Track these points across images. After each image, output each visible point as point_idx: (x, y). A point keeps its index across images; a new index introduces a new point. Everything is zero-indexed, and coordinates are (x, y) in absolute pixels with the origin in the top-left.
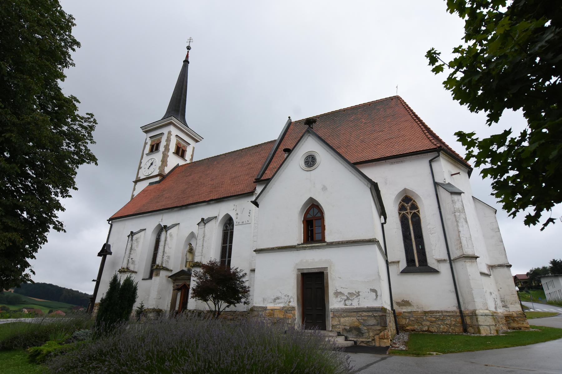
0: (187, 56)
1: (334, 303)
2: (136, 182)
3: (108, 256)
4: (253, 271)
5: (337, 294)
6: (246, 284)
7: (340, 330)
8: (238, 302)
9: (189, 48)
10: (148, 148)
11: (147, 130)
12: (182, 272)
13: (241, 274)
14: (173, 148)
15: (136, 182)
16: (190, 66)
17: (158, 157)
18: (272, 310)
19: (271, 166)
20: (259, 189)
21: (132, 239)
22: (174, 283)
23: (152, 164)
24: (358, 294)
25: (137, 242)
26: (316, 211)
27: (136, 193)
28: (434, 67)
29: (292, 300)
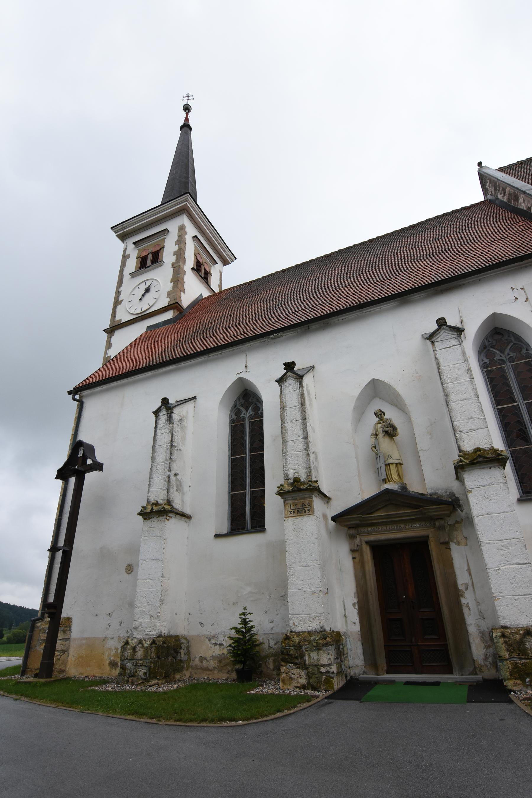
2: (111, 331)
9: (187, 108)
10: (132, 264)
11: (124, 231)
14: (190, 263)
15: (111, 331)
16: (196, 138)
17: (161, 277)
19: (158, 443)
21: (170, 419)
22: (352, 537)
23: (147, 290)
25: (183, 428)
27: (113, 353)
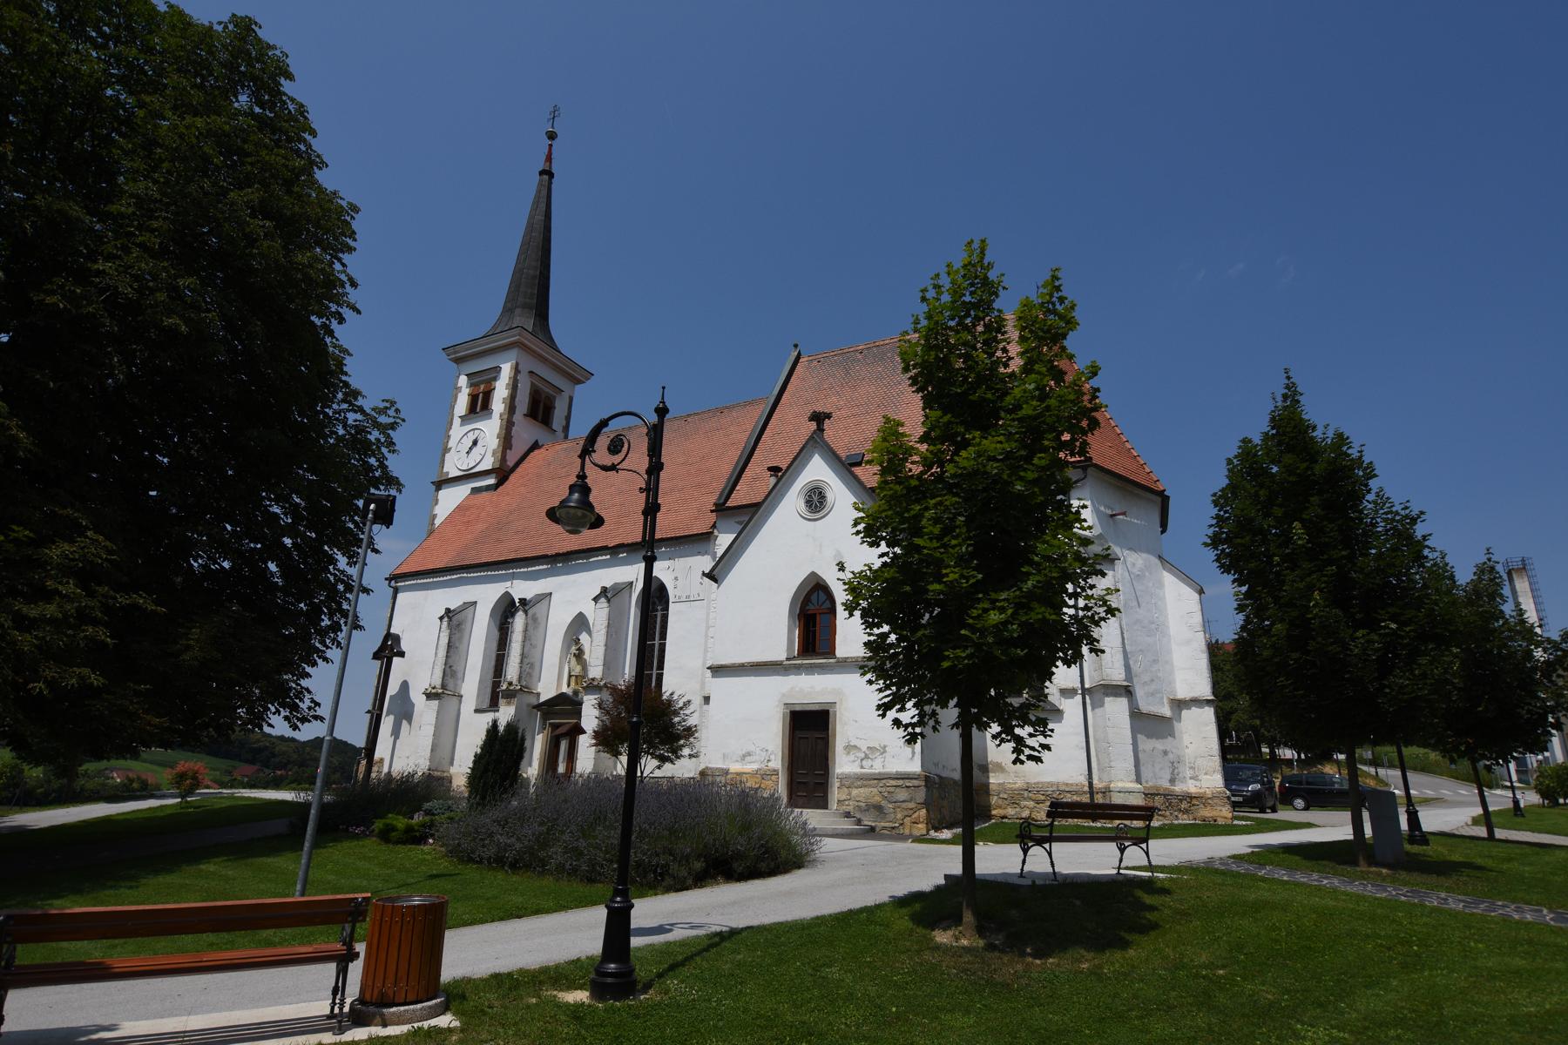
0: (549, 158)
1: (844, 764)
3: (396, 660)
4: (707, 699)
5: (850, 748)
6: (691, 721)
8: (678, 757)
9: (552, 136)
12: (561, 699)
20: (724, 540)
23: (475, 443)
24: (883, 750)
26: (823, 597)
28: (841, 596)
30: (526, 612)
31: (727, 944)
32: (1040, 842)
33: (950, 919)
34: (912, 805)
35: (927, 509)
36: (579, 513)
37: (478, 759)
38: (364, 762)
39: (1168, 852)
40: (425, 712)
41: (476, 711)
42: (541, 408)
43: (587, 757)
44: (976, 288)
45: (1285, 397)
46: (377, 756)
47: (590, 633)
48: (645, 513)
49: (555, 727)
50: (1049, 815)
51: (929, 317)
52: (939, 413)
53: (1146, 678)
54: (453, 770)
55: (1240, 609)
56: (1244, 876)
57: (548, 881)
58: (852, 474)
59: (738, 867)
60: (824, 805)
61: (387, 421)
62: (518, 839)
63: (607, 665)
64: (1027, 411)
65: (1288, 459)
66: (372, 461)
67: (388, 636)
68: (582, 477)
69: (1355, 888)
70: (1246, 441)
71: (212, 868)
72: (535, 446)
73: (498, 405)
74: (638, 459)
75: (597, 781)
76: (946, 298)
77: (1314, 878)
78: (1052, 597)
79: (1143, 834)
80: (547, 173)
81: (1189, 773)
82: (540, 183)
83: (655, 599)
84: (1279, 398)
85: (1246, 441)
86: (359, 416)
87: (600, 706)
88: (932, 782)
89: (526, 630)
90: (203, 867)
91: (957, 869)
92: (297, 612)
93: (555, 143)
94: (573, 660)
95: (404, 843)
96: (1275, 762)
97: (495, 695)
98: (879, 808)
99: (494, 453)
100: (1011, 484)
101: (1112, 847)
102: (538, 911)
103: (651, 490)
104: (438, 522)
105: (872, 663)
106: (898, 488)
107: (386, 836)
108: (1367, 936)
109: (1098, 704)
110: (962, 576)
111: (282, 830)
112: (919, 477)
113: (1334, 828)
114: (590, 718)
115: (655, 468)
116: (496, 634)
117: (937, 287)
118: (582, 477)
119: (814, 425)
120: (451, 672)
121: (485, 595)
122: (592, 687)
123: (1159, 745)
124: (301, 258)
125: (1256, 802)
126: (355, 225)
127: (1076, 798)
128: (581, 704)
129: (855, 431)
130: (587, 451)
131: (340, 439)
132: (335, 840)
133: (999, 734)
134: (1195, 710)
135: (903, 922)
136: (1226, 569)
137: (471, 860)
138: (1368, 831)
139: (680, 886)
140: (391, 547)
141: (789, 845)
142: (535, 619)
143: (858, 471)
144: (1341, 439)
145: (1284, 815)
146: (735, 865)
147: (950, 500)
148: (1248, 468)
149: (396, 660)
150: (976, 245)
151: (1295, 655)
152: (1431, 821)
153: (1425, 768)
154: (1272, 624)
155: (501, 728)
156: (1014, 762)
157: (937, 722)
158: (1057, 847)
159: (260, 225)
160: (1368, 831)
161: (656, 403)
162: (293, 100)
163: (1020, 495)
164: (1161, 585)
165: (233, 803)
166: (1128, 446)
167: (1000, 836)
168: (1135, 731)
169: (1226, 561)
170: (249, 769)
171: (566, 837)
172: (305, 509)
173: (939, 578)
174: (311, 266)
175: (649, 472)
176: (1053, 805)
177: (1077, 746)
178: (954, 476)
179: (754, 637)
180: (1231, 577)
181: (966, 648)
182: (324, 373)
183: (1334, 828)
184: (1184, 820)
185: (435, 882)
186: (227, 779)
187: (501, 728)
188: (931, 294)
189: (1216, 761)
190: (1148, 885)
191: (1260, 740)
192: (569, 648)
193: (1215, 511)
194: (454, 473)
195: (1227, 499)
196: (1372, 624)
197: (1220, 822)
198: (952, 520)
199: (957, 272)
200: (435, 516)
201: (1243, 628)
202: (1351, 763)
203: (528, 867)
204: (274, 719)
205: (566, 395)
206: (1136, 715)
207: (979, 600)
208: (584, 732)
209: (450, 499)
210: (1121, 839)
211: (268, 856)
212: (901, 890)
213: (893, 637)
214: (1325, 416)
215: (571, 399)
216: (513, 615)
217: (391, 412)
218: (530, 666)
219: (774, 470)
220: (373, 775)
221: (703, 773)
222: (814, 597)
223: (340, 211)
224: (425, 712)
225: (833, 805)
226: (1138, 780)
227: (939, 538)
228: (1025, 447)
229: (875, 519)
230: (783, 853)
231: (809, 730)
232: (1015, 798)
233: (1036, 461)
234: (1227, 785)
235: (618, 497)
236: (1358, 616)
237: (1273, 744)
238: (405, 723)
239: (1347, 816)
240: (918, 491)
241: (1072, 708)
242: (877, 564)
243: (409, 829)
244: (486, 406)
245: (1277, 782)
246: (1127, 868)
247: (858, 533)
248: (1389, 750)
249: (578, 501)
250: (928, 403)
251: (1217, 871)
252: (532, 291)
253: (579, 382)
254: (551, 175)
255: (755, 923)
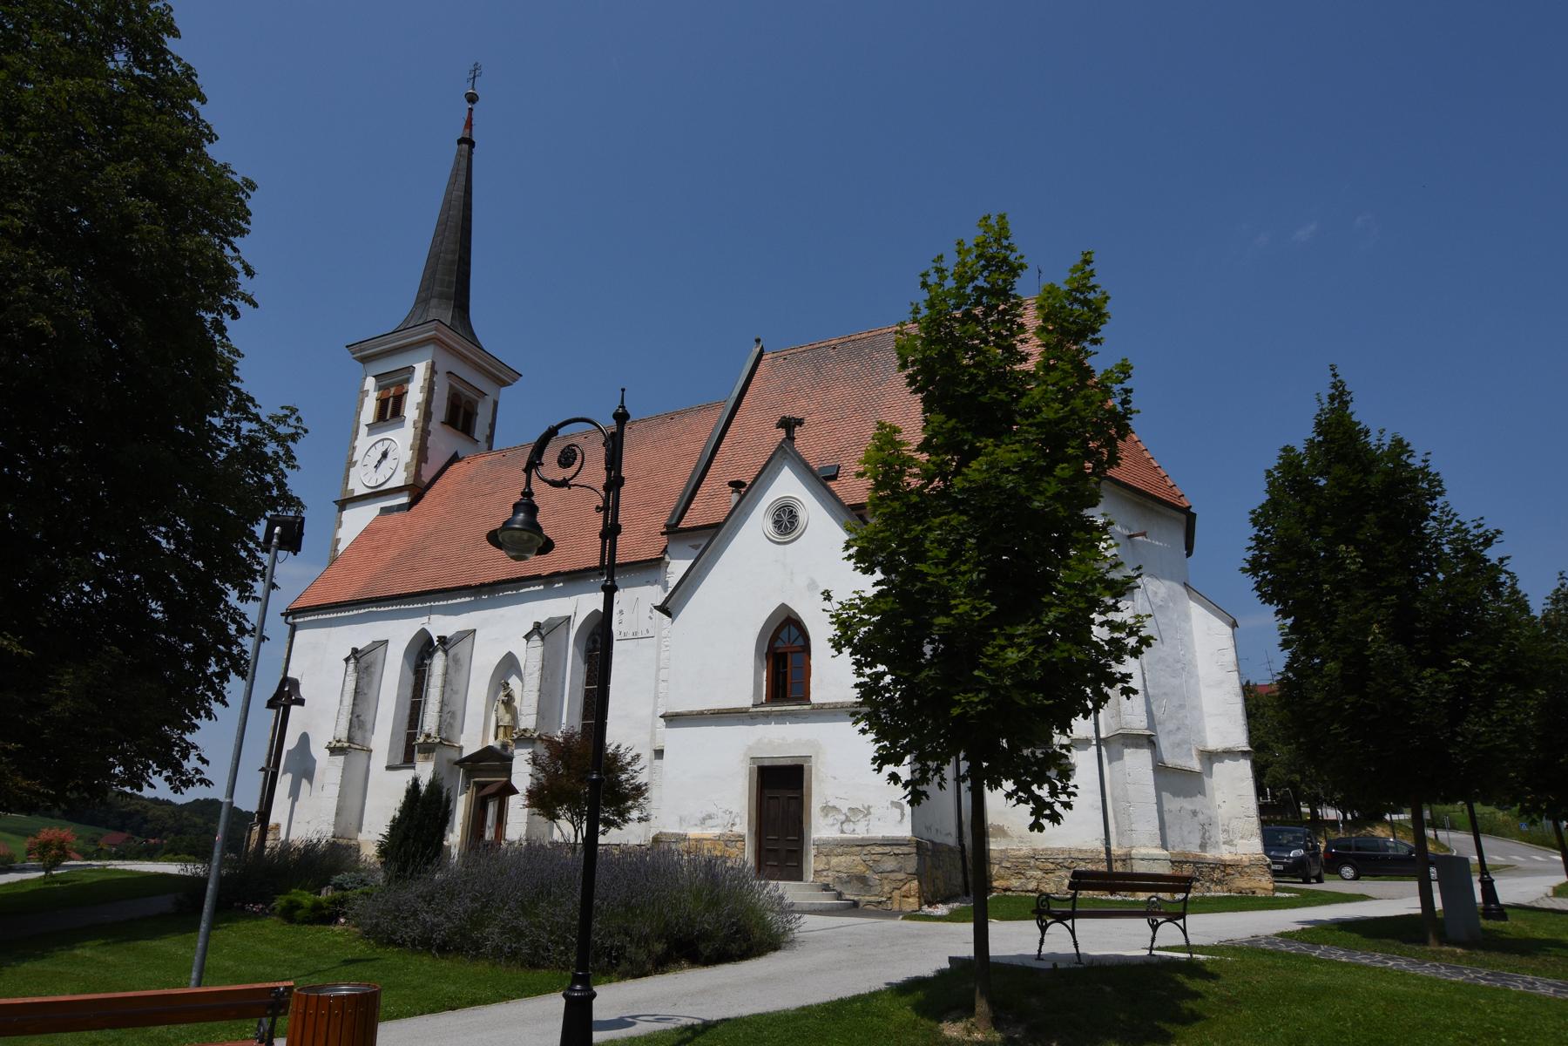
0: (469, 124)
1: (821, 829)
3: (293, 708)
4: (659, 753)
5: (828, 809)
6: (641, 779)
7: (829, 880)
8: (626, 821)
9: (472, 99)
12: (487, 753)
13: (628, 759)
18: (697, 840)
20: (677, 568)
23: (385, 455)
24: (867, 812)
28: (821, 631)
29: (737, 820)
30: (446, 652)
31: (701, 1040)
32: (1060, 918)
33: (962, 1009)
34: (901, 876)
35: (930, 529)
36: (526, 535)
37: (396, 825)
38: (257, 828)
39: (1208, 928)
40: (329, 770)
41: (389, 768)
42: (460, 414)
43: (518, 820)
44: (997, 265)
45: (1332, 398)
46: (272, 821)
47: (520, 676)
48: (603, 536)
49: (481, 786)
50: (1071, 886)
51: (931, 306)
52: (943, 417)
53: (1171, 726)
54: (361, 837)
55: (1285, 644)
56: (1297, 957)
57: (482, 967)
58: (828, 489)
59: (706, 949)
60: (796, 874)
61: (288, 431)
62: (448, 917)
63: (541, 713)
64: (1048, 414)
65: (1338, 470)
66: (269, 478)
67: (285, 680)
68: (528, 494)
69: (1426, 970)
70: (1287, 450)
71: (88, 953)
72: (455, 459)
73: (411, 411)
74: (594, 471)
75: (533, 850)
76: (950, 284)
77: (1377, 959)
78: (1078, 628)
79: (1179, 908)
80: (467, 142)
81: (1222, 837)
82: (459, 154)
83: (598, 641)
84: (1326, 400)
85: (1287, 450)
86: (255, 426)
87: (534, 761)
88: (925, 849)
89: (446, 673)
90: (78, 952)
91: (968, 951)
92: (180, 654)
93: (476, 107)
94: (502, 708)
95: (311, 922)
96: (1317, 824)
97: (410, 749)
98: (862, 880)
99: (407, 467)
100: (1029, 499)
101: (1143, 923)
102: (473, 1002)
103: (610, 509)
104: (341, 548)
105: (866, 709)
106: (896, 504)
107: (290, 914)
108: (1447, 1027)
109: (1116, 757)
110: (974, 608)
111: (176, 907)
112: (919, 491)
113: (1397, 900)
114: (522, 774)
115: (614, 484)
116: (411, 678)
117: (939, 271)
118: (528, 494)
119: (782, 433)
120: (359, 722)
121: (399, 633)
122: (524, 739)
123: (1187, 804)
124: (188, 243)
125: (1297, 870)
126: (249, 205)
127: (1090, 867)
128: (511, 759)
129: (841, 438)
130: (533, 464)
131: (232, 453)
132: (229, 920)
133: (1015, 792)
134: (1228, 764)
135: (904, 1013)
136: (1267, 598)
137: (392, 942)
138: (1438, 904)
139: (639, 972)
140: (293, 575)
141: (766, 927)
142: (456, 660)
143: (832, 485)
144: (1400, 446)
145: (1331, 885)
146: (702, 947)
147: (956, 518)
148: (1291, 479)
149: (293, 708)
150: (993, 221)
151: (1350, 699)
152: (1509, 891)
153: (1495, 832)
154: (1323, 663)
155: (423, 788)
156: (1032, 828)
157: (942, 779)
158: (1081, 925)
159: (139, 206)
160: (1438, 904)
161: (614, 407)
162: (178, 60)
163: (1036, 511)
164: (1187, 617)
165: (108, 877)
166: (1148, 455)
167: (1015, 909)
168: (1159, 789)
169: (1268, 589)
170: (119, 837)
171: (504, 915)
172: (190, 534)
173: (946, 610)
174: (201, 253)
175: (607, 488)
176: (1076, 875)
177: (1103, 805)
178: (962, 490)
179: (723, 676)
180: (1274, 608)
181: (979, 691)
182: (210, 378)
183: (1397, 900)
184: (1217, 892)
185: (351, 968)
186: (91, 849)
187: (423, 788)
188: (933, 279)
189: (1253, 824)
190: (1192, 969)
191: (1298, 797)
192: (496, 693)
193: (1255, 531)
194: (360, 490)
195: (1267, 518)
196: (1442, 663)
197: (1260, 893)
198: (961, 542)
199: (969, 251)
200: (338, 541)
201: (1288, 667)
202: (1419, 824)
203: (459, 950)
204: (156, 780)
205: (489, 400)
206: (1161, 769)
207: (994, 637)
208: (515, 792)
209: (356, 521)
210: (1151, 913)
211: (152, 938)
212: (899, 975)
213: (888, 679)
214: (1378, 421)
215: (496, 404)
216: (431, 656)
217: (292, 421)
218: (451, 715)
219: (737, 485)
220: (268, 843)
221: (656, 840)
222: (784, 634)
223: (234, 188)
224: (329, 770)
225: (809, 876)
226: (1164, 846)
227: (946, 563)
228: (1045, 456)
229: (871, 541)
230: (757, 933)
231: (781, 789)
232: (1019, 867)
233: (1058, 472)
234: (1266, 852)
235: (570, 519)
236: (1424, 653)
237: (1315, 803)
238: (304, 782)
239: (1413, 886)
240: (918, 509)
241: (1084, 763)
242: (870, 592)
243: (317, 907)
244: (397, 412)
245: (1322, 846)
246: (1159, 949)
247: (850, 557)
248: (1458, 809)
249: (524, 522)
250: (929, 405)
251: (1264, 952)
252: (450, 277)
253: (504, 384)
254: (471, 144)
255: (731, 1014)
